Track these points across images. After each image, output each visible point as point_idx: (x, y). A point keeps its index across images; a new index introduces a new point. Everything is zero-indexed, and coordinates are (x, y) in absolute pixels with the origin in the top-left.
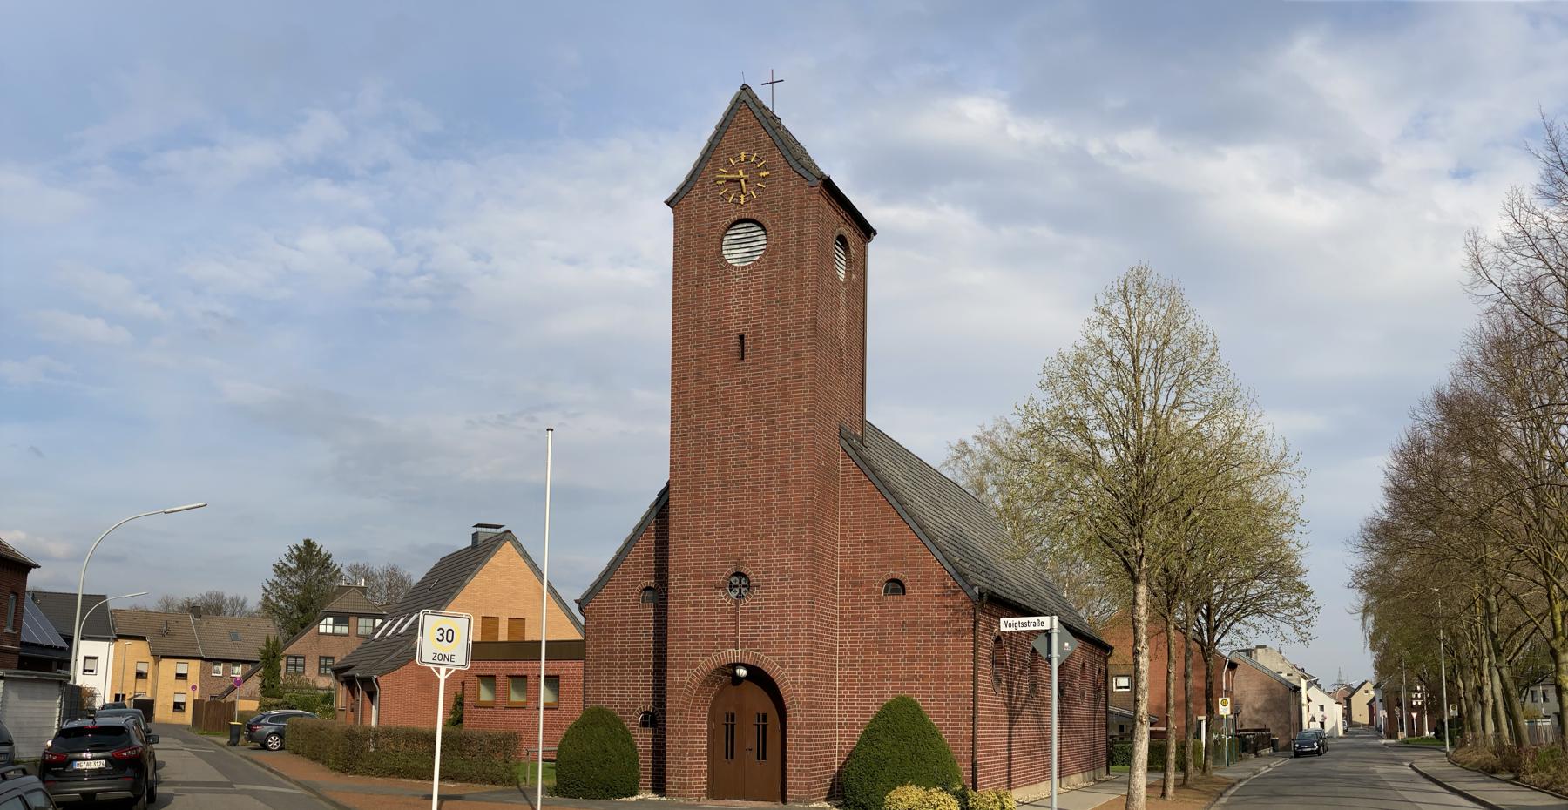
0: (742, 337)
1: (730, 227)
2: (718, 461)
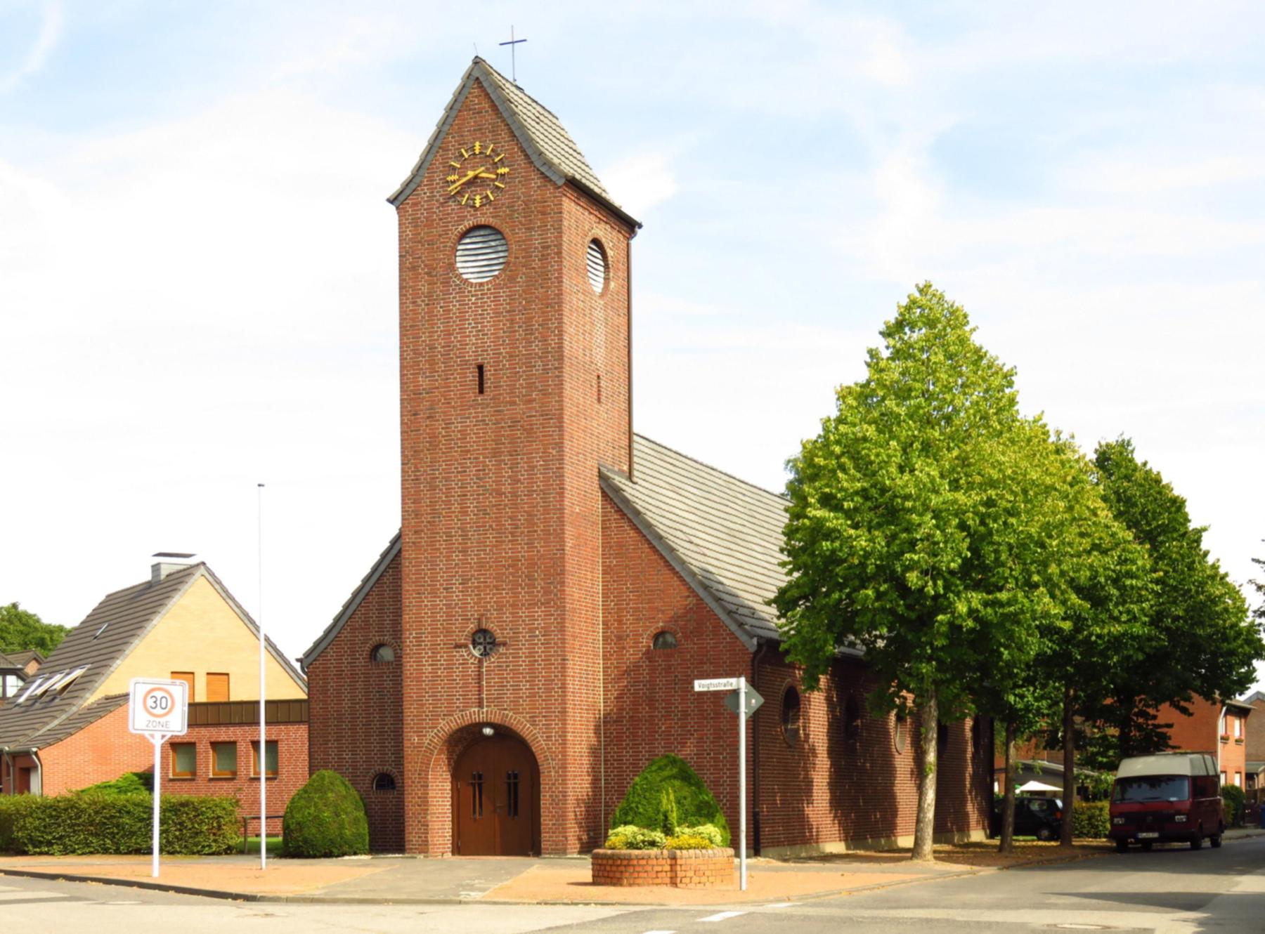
0: (480, 368)
1: (464, 235)
2: (456, 507)
